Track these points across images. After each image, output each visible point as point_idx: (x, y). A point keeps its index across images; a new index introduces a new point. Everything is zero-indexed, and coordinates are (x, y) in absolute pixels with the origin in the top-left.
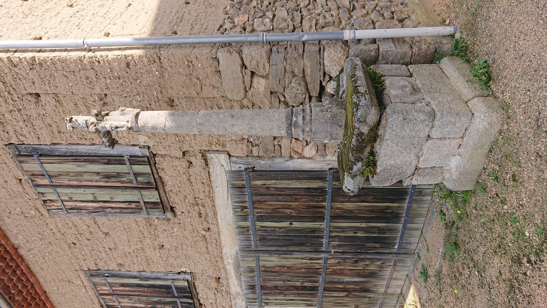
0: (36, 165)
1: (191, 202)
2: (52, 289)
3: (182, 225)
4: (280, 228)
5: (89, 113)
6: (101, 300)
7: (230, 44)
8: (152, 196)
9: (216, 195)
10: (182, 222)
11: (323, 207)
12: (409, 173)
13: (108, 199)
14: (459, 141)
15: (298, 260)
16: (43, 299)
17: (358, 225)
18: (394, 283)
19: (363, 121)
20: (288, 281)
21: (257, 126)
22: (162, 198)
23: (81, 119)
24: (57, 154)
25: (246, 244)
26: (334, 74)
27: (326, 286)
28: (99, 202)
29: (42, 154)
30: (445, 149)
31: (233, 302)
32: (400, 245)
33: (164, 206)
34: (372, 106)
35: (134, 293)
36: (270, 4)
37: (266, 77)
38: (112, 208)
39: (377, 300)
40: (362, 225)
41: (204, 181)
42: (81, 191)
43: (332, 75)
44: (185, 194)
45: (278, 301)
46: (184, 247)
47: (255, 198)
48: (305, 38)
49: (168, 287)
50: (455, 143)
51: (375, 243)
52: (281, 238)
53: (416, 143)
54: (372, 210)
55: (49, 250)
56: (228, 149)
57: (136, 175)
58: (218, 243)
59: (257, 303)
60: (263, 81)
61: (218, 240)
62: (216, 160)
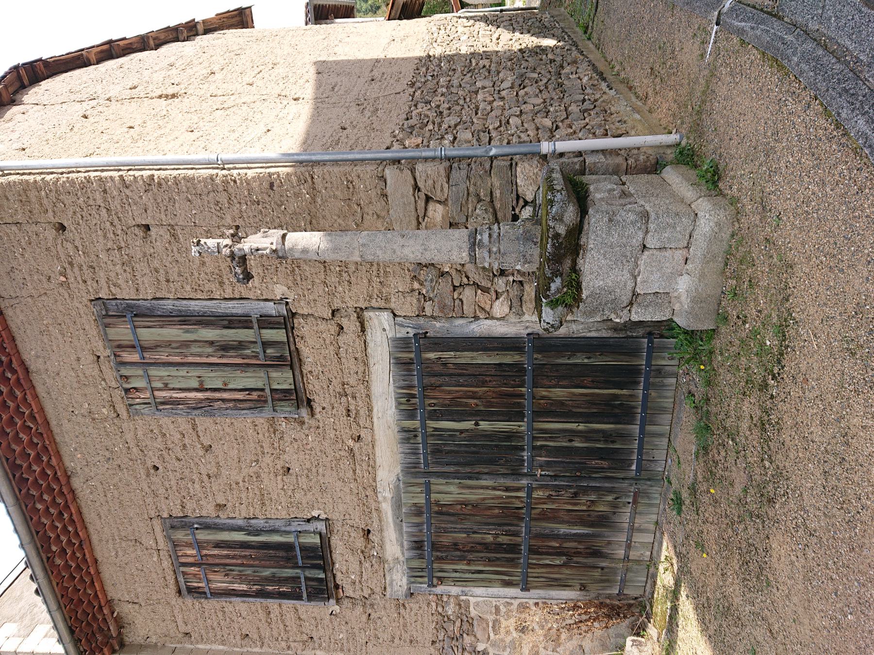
0: (126, 331)
1: (338, 390)
2: (106, 555)
3: (321, 430)
4: (461, 431)
5: (222, 236)
6: (181, 579)
7: (399, 161)
8: (282, 379)
9: (374, 377)
10: (321, 425)
11: (521, 396)
12: (625, 299)
13: (220, 385)
14: (685, 252)
15: (486, 490)
16: (92, 573)
17: (573, 426)
18: (638, 538)
19: (559, 219)
20: (474, 532)
21: (433, 247)
22: (297, 384)
23: (211, 243)
24: (159, 313)
25: (412, 461)
26: (529, 197)
27: (533, 542)
28: (207, 390)
29: (136, 313)
30: (667, 265)
31: (388, 578)
32: (640, 461)
33: (298, 398)
34: (569, 203)
35: (234, 561)
36: (450, 127)
37: (443, 203)
38: (223, 400)
39: (614, 571)
40: (580, 428)
41: (358, 355)
42: (183, 372)
43: (527, 199)
44: (330, 376)
45: (457, 575)
46: (320, 470)
47: (426, 381)
48: (493, 152)
49: (288, 547)
50: (679, 255)
51: (601, 459)
52: (463, 449)
53: (628, 254)
54: (592, 401)
55: (117, 479)
56: (393, 306)
57: (266, 344)
58: (371, 462)
59: (426, 579)
60: (440, 208)
61: (371, 456)
62: (376, 321)
